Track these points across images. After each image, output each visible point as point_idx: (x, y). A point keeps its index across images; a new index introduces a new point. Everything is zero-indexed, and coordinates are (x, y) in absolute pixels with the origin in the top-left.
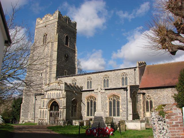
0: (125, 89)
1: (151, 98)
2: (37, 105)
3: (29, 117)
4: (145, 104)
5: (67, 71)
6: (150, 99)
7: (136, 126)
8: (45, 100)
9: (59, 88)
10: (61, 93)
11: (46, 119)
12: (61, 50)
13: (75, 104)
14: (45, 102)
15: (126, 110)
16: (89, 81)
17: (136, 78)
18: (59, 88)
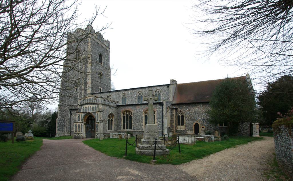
2: (72, 119)
3: (65, 131)
4: (177, 118)
5: (101, 88)
6: (181, 114)
7: (186, 140)
8: (81, 114)
10: (97, 107)
11: (82, 132)
13: (112, 118)
14: (81, 116)
15: (161, 123)
16: (124, 97)
17: (169, 94)
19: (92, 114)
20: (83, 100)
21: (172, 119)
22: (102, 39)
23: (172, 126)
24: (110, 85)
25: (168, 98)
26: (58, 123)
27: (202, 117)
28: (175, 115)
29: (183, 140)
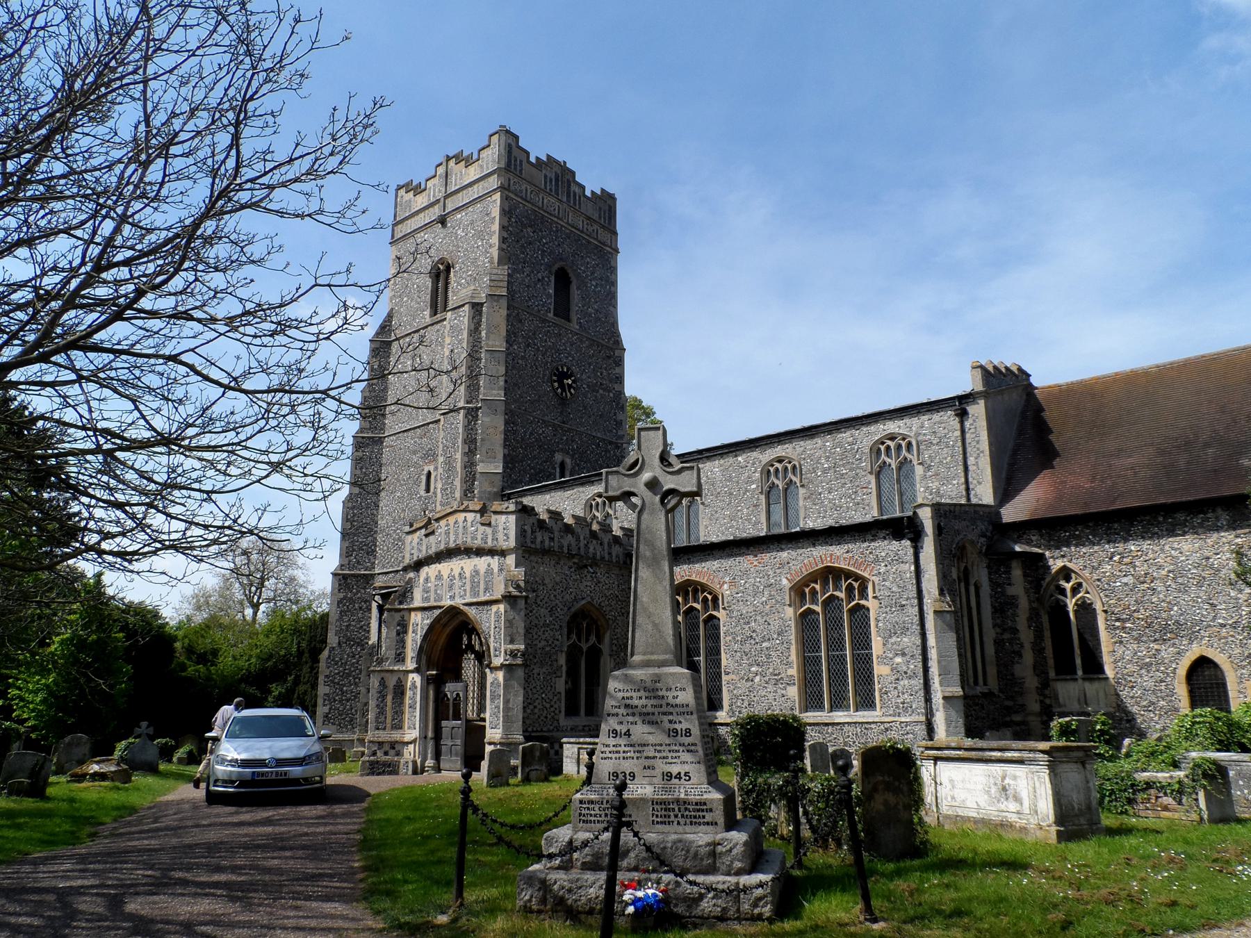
0: (905, 528)
1: (1080, 585)
4: (1046, 625)
5: (568, 461)
6: (1075, 590)
7: (1017, 799)
9: (485, 540)
10: (496, 570)
12: (528, 345)
13: (593, 639)
17: (971, 460)
18: (485, 540)
19: (465, 614)
20: (427, 536)
21: (1004, 630)
22: (574, 188)
23: (1010, 682)
24: (622, 437)
25: (968, 489)
26: (330, 681)
27: (1238, 607)
28: (1024, 603)
29: (993, 790)
